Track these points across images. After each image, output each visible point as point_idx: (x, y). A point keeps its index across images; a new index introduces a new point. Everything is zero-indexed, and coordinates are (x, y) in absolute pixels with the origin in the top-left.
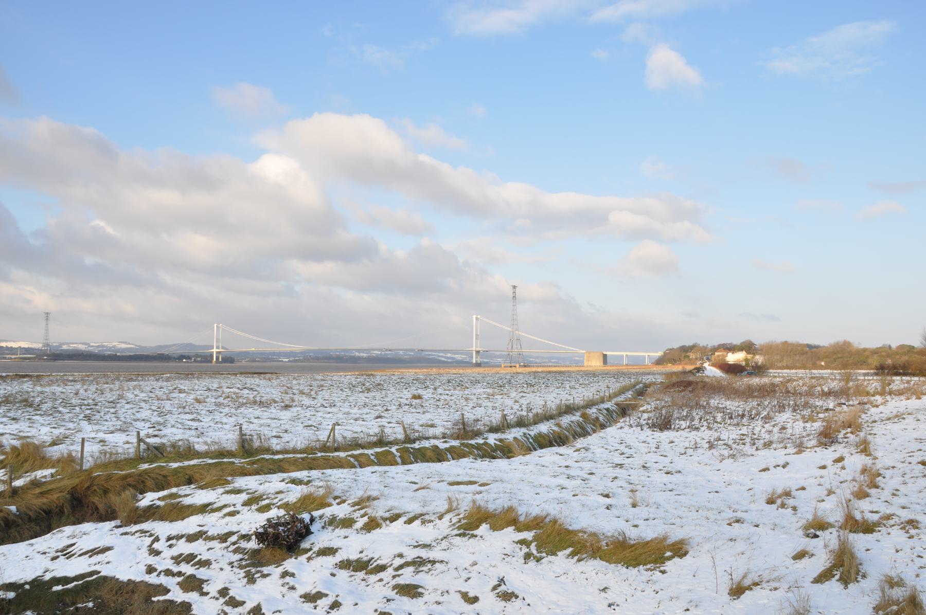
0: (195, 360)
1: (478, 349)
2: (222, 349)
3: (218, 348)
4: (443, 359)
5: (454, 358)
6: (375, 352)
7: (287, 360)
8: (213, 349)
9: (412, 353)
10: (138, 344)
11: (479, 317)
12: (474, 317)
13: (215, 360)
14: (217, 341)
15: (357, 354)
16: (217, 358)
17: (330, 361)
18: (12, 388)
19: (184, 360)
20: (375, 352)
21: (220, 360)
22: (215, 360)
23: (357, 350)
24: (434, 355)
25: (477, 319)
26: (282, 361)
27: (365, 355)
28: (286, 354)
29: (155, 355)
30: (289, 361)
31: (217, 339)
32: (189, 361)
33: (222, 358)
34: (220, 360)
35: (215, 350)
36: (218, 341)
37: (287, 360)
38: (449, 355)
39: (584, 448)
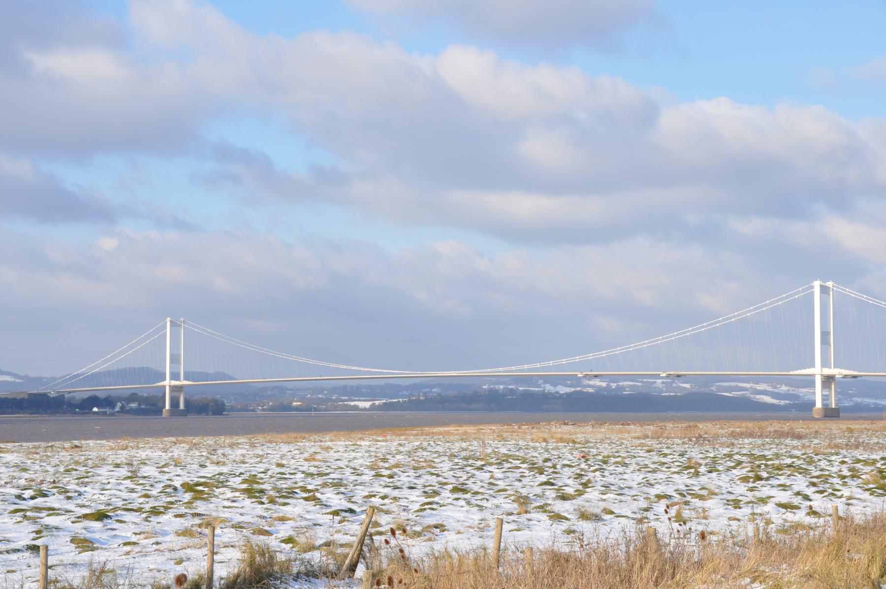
0: (122, 408)
1: (827, 371)
2: (185, 379)
3: (175, 376)
4: (767, 399)
5: (798, 397)
6: (592, 383)
7: (367, 405)
8: (165, 380)
9: (687, 386)
10: (22, 374)
11: (830, 284)
12: (817, 284)
13: (167, 407)
14: (172, 362)
15: (549, 388)
16: (175, 403)
17: (473, 406)
18: (1, 532)
19: (95, 409)
20: (592, 383)
21: (182, 406)
22: (167, 407)
23: (547, 379)
24: (742, 389)
25: (824, 290)
26: (356, 408)
27: (563, 390)
28: (371, 392)
29: (19, 397)
30: (373, 408)
31: (171, 355)
32: (108, 410)
33: (187, 402)
34: (182, 406)
35: (167, 383)
36: (175, 359)
37: (367, 405)
38: (784, 388)
39: (24, 499)
